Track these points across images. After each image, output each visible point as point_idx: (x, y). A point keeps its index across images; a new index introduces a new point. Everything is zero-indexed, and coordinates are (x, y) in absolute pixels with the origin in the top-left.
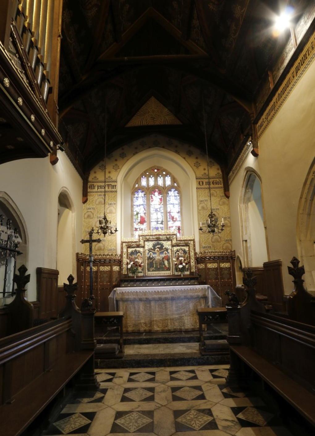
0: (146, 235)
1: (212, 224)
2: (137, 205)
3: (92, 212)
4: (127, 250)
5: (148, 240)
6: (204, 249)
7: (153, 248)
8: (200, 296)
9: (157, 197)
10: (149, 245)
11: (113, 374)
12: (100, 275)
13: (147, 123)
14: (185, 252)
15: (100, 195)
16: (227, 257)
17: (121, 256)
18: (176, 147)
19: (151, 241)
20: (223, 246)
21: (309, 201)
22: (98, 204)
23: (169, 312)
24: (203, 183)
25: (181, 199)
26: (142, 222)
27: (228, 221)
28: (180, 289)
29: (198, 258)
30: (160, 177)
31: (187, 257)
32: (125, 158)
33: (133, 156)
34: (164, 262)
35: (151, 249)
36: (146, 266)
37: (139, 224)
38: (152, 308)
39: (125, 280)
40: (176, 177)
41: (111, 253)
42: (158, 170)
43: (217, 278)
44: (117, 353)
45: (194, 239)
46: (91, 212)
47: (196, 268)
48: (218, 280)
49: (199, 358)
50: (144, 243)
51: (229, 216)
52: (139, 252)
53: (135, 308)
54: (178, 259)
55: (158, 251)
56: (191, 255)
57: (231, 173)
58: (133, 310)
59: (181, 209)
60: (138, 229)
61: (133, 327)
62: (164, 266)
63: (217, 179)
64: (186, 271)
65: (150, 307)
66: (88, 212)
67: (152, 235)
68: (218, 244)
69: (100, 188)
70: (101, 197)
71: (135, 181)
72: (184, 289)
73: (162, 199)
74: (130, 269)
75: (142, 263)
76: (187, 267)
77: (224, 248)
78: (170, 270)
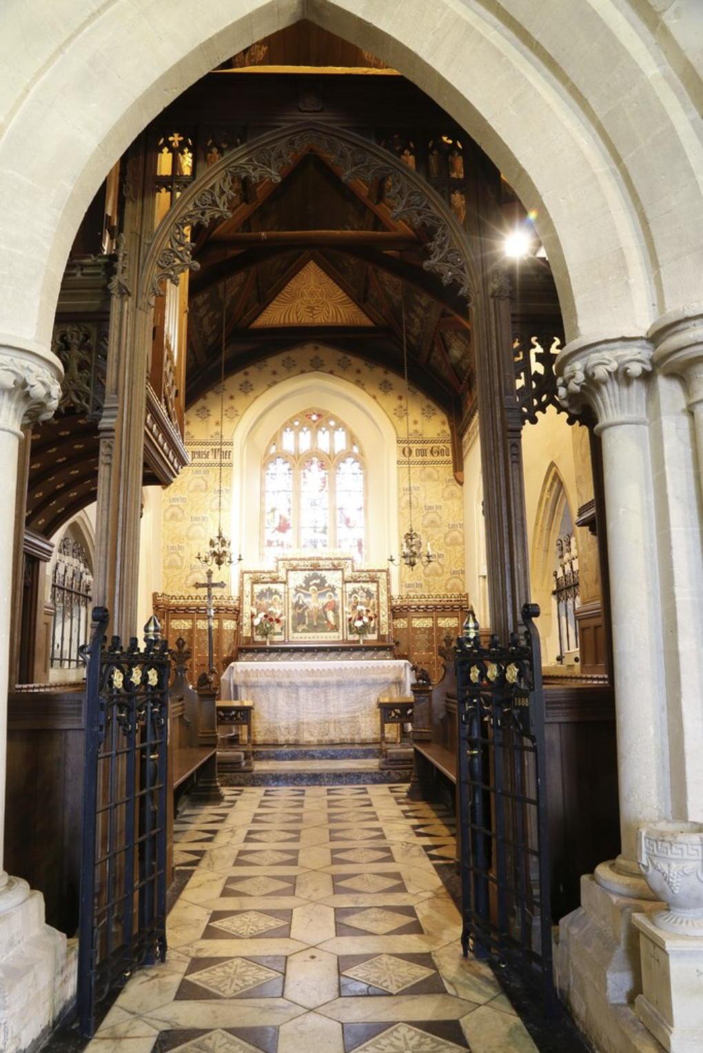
0: (291, 560)
1: (412, 551)
2: (273, 492)
3: (181, 506)
4: (252, 589)
5: (295, 569)
6: (408, 589)
7: (304, 585)
8: (390, 680)
10: (297, 579)
11: (241, 791)
13: (298, 318)
14: (369, 594)
15: (197, 472)
17: (240, 599)
18: (358, 372)
19: (301, 570)
20: (446, 584)
21: (545, 532)
23: (332, 709)
24: (410, 452)
26: (283, 527)
27: (460, 533)
28: (353, 667)
29: (394, 607)
30: (324, 432)
31: (374, 605)
32: (250, 394)
33: (267, 390)
34: (325, 613)
35: (301, 587)
36: (290, 622)
37: (277, 532)
38: (301, 700)
39: (247, 649)
40: (356, 432)
41: (221, 594)
42: (319, 416)
43: (429, 649)
45: (388, 569)
46: (178, 506)
47: (389, 627)
48: (433, 651)
49: (376, 773)
50: (287, 574)
51: (461, 523)
52: (276, 593)
53: (268, 700)
54: (354, 608)
55: (315, 592)
56: (381, 600)
57: (466, 437)
58: (265, 704)
59: (366, 502)
60: (275, 544)
61: (266, 734)
62: (326, 622)
63: (441, 445)
64: (369, 633)
65: (297, 698)
66: (172, 506)
67: (304, 559)
68: (437, 578)
69: (196, 456)
70: (199, 476)
71: (269, 440)
72: (362, 668)
73: (327, 479)
74: (257, 627)
75: (281, 615)
76: (372, 625)
77: (449, 587)
78: (337, 630)
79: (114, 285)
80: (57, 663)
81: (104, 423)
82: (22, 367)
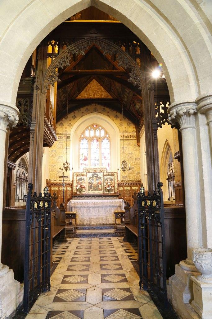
7: (92, 177)
9: (95, 143)
10: (90, 175)
12: (60, 193)
14: (111, 179)
16: (136, 183)
17: (73, 181)
18: (108, 112)
19: (91, 172)
22: (58, 148)
25: (110, 144)
34: (98, 185)
35: (91, 177)
36: (88, 188)
37: (84, 161)
39: (75, 196)
40: (108, 131)
42: (96, 126)
44: (74, 231)
47: (118, 190)
52: (83, 179)
54: (107, 184)
57: (141, 132)
59: (110, 152)
60: (83, 164)
61: (80, 222)
67: (92, 169)
75: (85, 186)
79: (35, 86)
80: (17, 200)
81: (32, 128)
82: (7, 111)
